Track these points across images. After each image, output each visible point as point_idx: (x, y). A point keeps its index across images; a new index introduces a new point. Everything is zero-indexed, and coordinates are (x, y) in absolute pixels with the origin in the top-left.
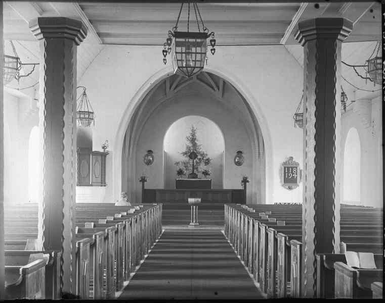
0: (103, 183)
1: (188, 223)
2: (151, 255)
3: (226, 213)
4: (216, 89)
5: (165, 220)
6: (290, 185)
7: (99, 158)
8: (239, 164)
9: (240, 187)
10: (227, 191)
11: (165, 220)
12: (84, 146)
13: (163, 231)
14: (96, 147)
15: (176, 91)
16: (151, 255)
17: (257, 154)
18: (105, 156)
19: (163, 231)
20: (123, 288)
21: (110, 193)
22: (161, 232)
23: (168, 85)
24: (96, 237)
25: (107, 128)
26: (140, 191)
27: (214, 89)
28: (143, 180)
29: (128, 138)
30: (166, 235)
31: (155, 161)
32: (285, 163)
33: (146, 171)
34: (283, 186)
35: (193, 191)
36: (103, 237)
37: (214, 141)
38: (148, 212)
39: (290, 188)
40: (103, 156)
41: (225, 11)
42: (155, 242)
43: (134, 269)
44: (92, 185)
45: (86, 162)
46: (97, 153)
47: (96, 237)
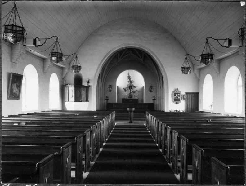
0: (87, 100)
1: (2, 162)
2: (114, 131)
3: (146, 115)
4: (140, 57)
5: (117, 119)
6: (177, 102)
7: (85, 89)
8: (151, 91)
9: (152, 102)
10: (146, 104)
11: (117, 119)
12: (78, 82)
13: (116, 124)
14: (85, 84)
15: (123, 58)
16: (114, 131)
17: (159, 87)
18: (88, 88)
19: (116, 124)
20: (100, 152)
21: (91, 105)
22: (114, 125)
23: (119, 55)
24: (92, 128)
25: (90, 73)
26: (106, 104)
27: (139, 58)
28: (107, 99)
29: (100, 77)
30: (117, 127)
31: (113, 90)
32: (174, 91)
33: (108, 94)
34: (173, 102)
35: (132, 106)
36: (95, 127)
37: (139, 80)
38: (110, 116)
39: (177, 103)
40: (88, 88)
41: (127, 85)
42: (101, 146)
43: (107, 137)
44: (81, 102)
45: (79, 91)
46: (84, 87)
47: (92, 128)
